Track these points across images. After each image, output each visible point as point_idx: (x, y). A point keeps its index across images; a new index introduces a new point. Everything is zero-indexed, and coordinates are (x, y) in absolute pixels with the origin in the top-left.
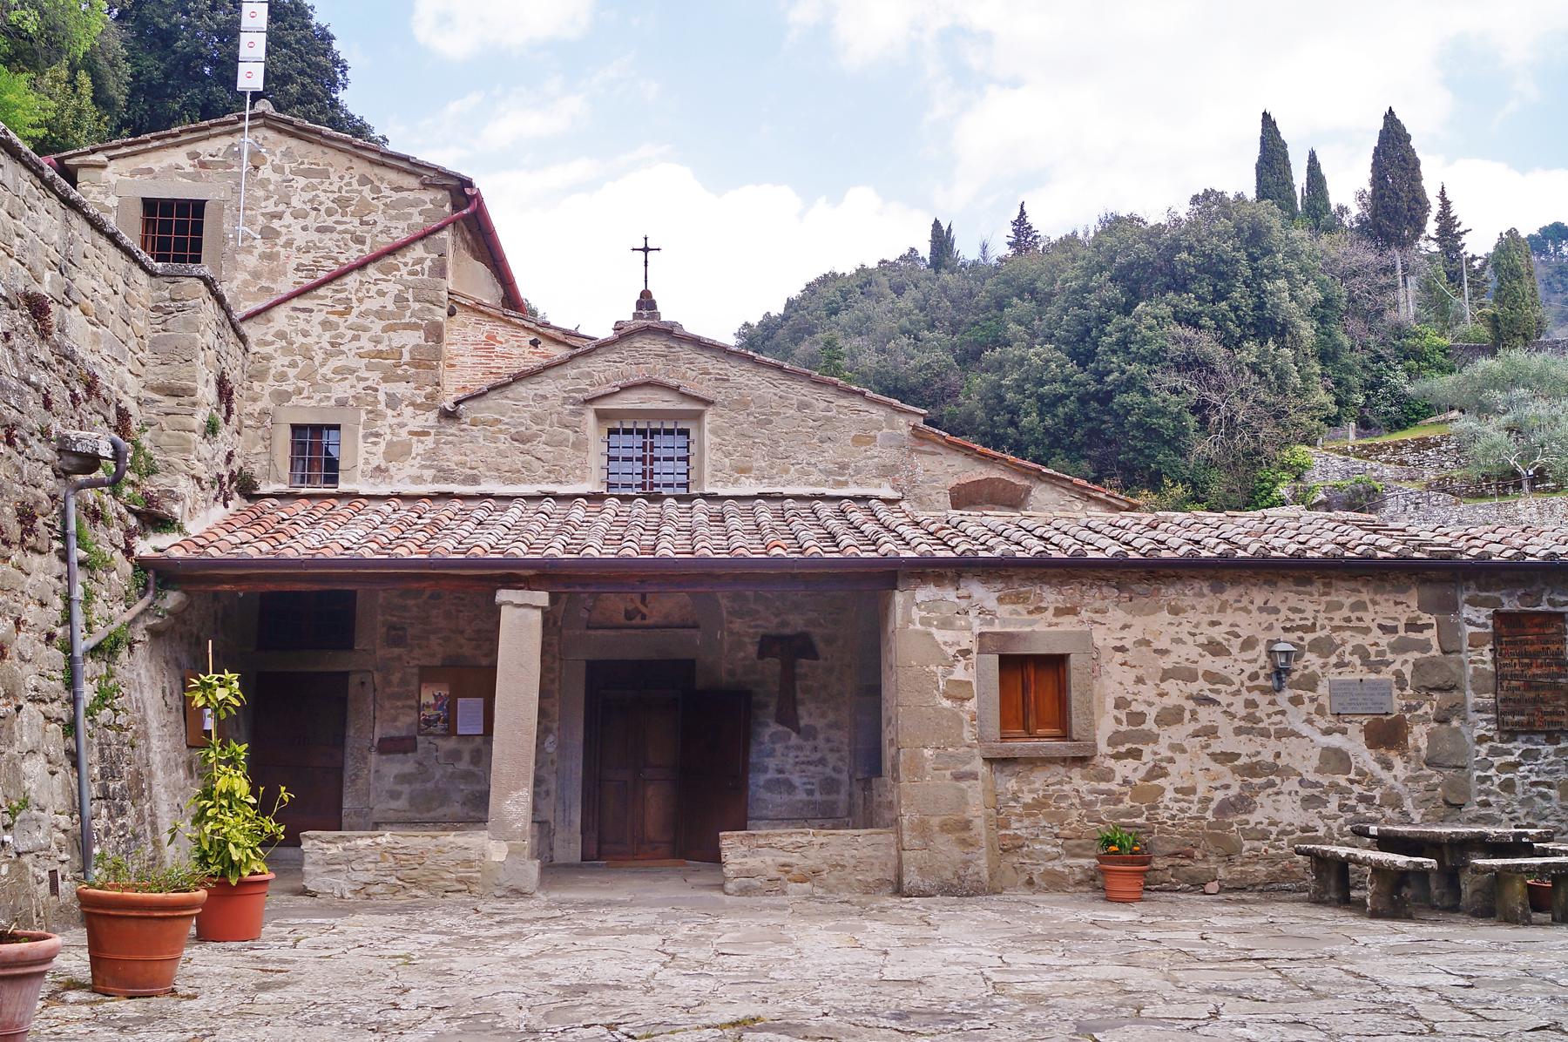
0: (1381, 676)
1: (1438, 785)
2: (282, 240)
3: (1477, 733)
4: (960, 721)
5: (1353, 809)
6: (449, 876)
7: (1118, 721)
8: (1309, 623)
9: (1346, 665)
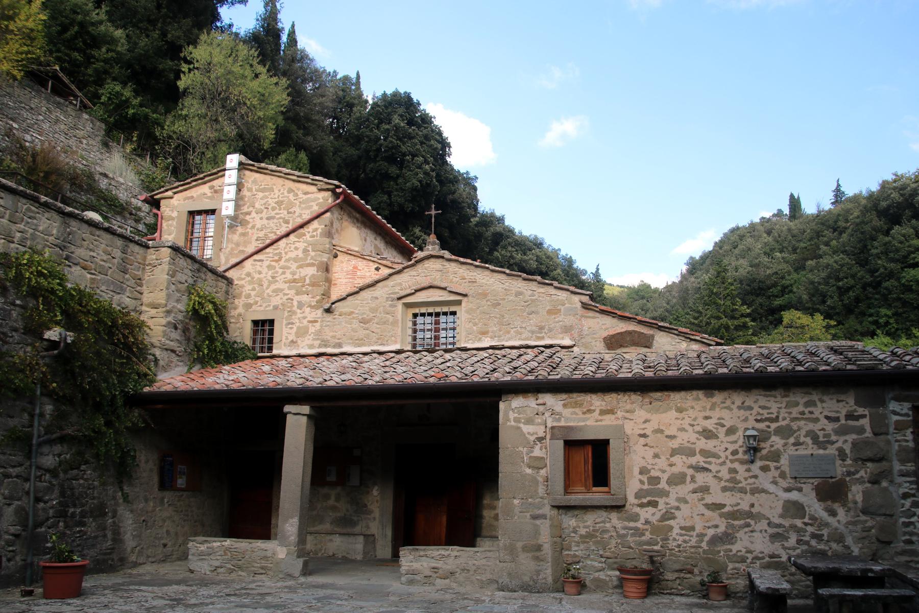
0: (827, 452)
1: (872, 527)
2: (250, 225)
3: (901, 491)
4: (537, 482)
5: (807, 543)
6: (256, 565)
7: (642, 482)
8: (774, 416)
9: (801, 444)
